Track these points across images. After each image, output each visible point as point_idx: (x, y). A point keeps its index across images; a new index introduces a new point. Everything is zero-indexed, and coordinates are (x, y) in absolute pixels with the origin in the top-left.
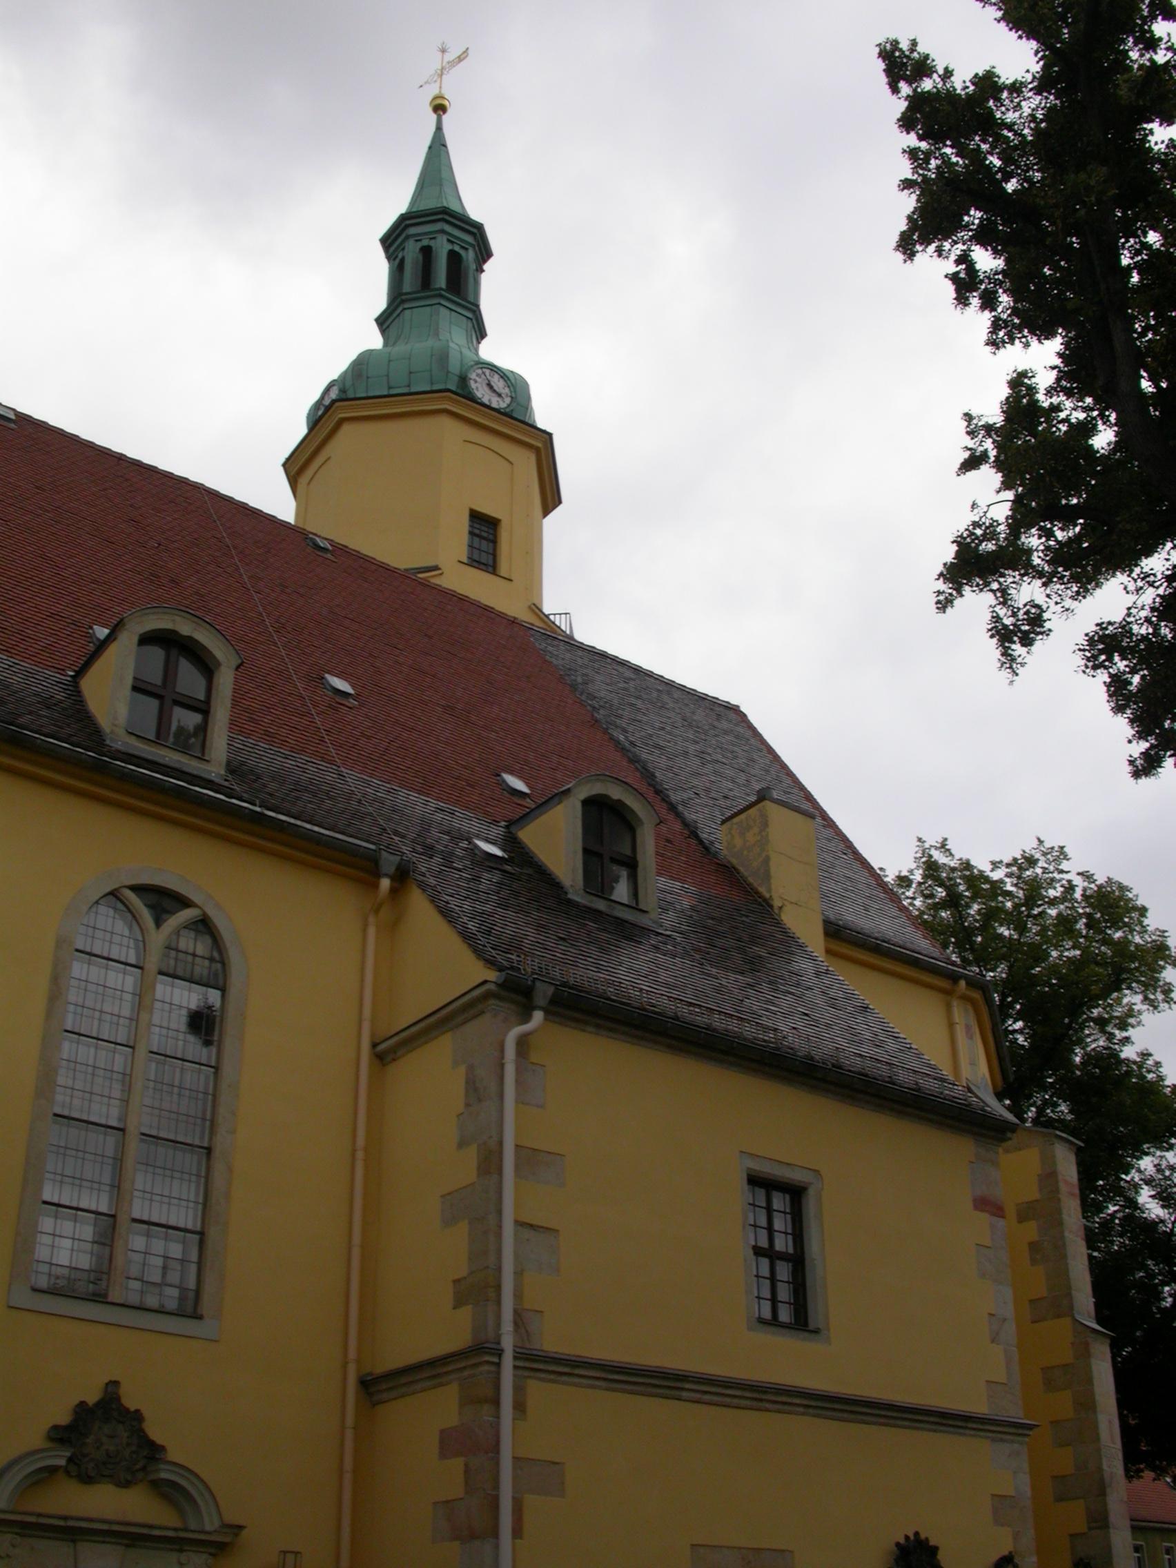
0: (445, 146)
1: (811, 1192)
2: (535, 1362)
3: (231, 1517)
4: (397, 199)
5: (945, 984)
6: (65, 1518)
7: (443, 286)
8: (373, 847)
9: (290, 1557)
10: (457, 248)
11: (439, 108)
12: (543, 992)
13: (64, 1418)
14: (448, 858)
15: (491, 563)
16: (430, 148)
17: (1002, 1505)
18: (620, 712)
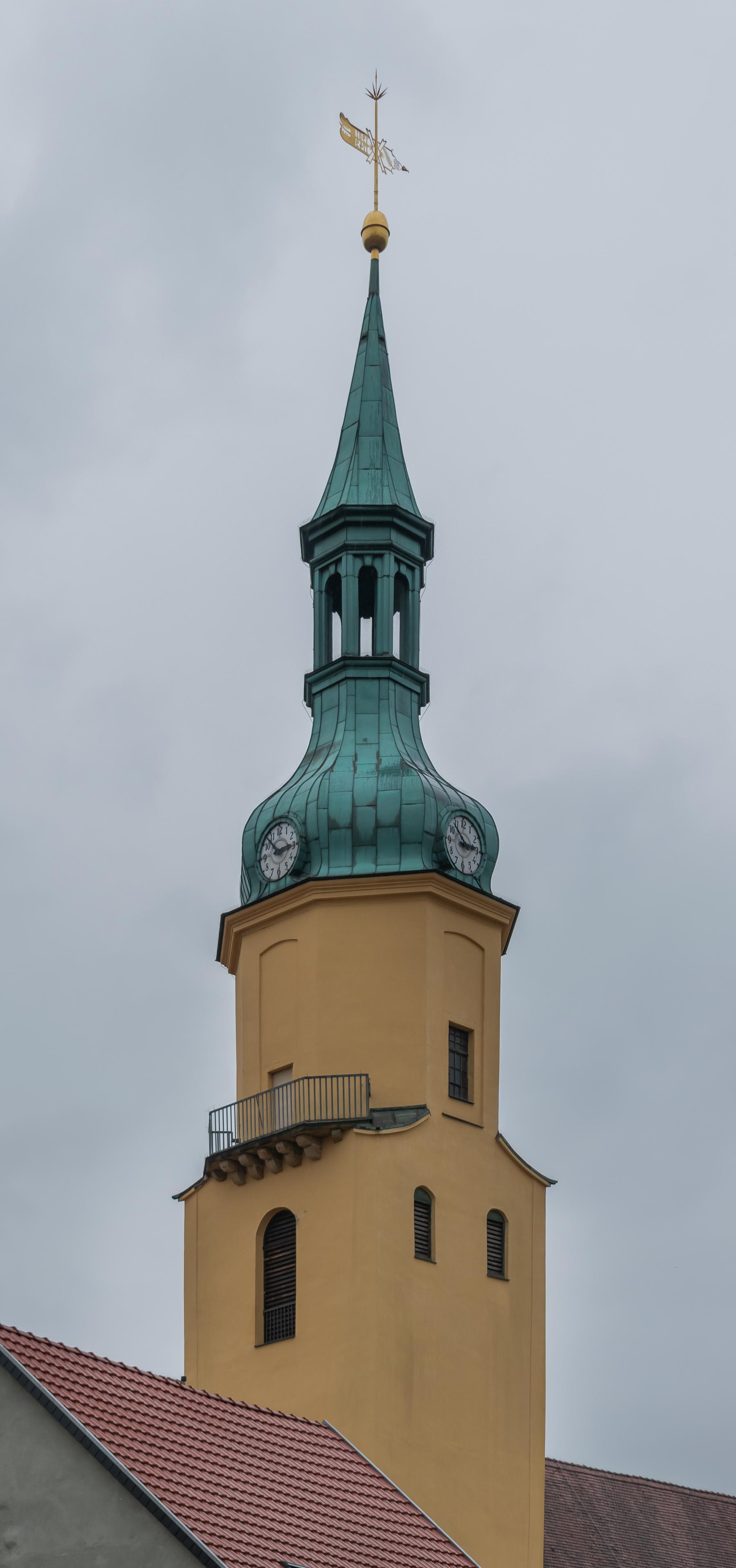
4: (304, 478)
10: (404, 570)
11: (375, 243)
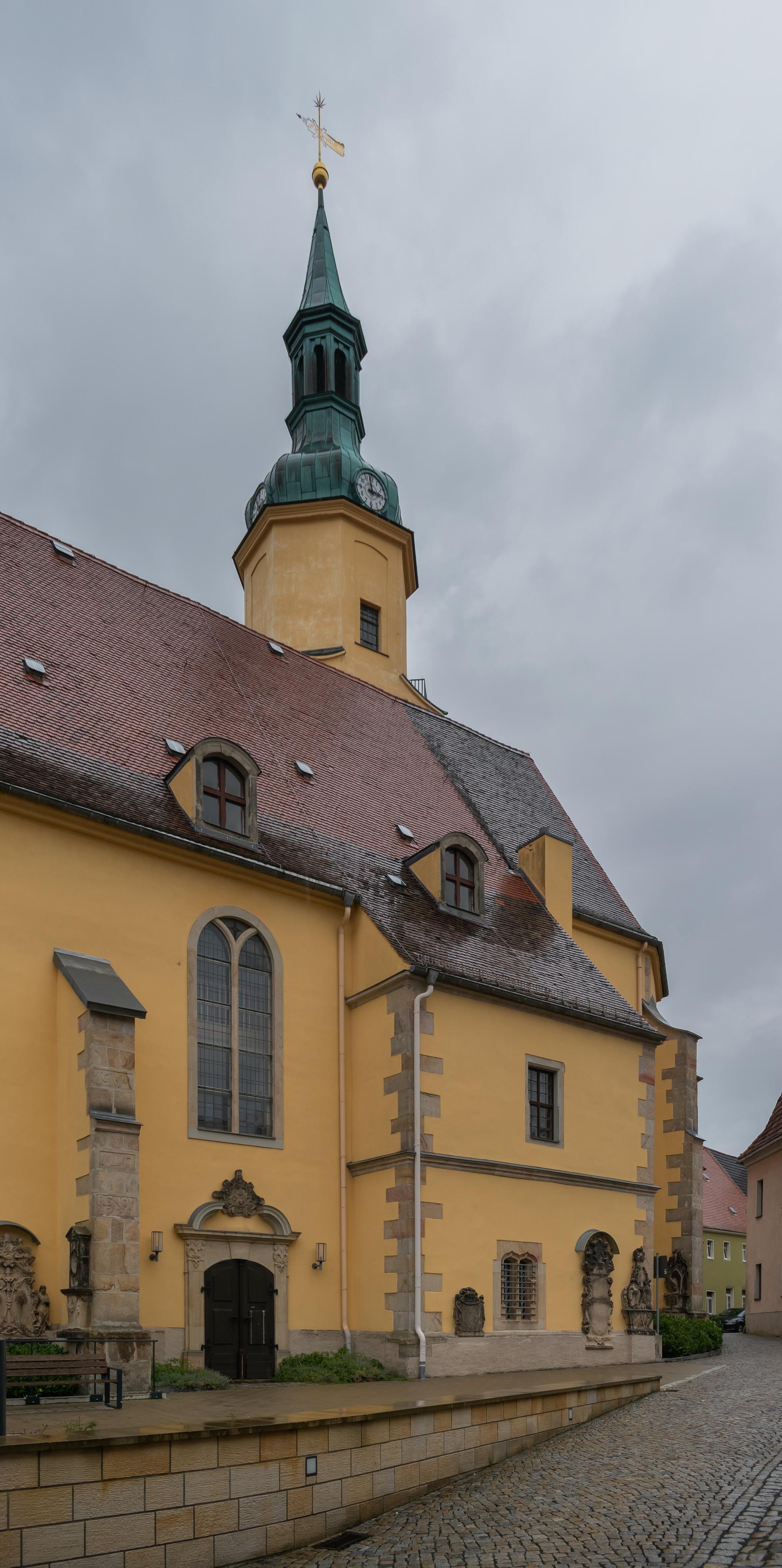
0: (326, 228)
1: (559, 1073)
2: (431, 1159)
3: (295, 1229)
5: (635, 944)
6: (225, 1232)
7: (334, 390)
8: (341, 889)
9: (321, 1246)
10: (341, 347)
11: (320, 181)
12: (434, 975)
13: (218, 1188)
14: (376, 888)
15: (374, 643)
16: (315, 231)
17: (639, 1226)
18: (459, 767)
